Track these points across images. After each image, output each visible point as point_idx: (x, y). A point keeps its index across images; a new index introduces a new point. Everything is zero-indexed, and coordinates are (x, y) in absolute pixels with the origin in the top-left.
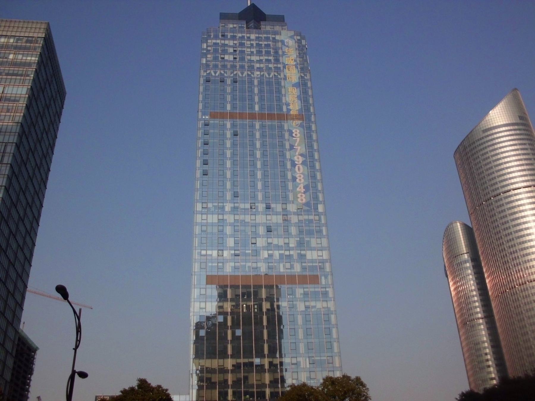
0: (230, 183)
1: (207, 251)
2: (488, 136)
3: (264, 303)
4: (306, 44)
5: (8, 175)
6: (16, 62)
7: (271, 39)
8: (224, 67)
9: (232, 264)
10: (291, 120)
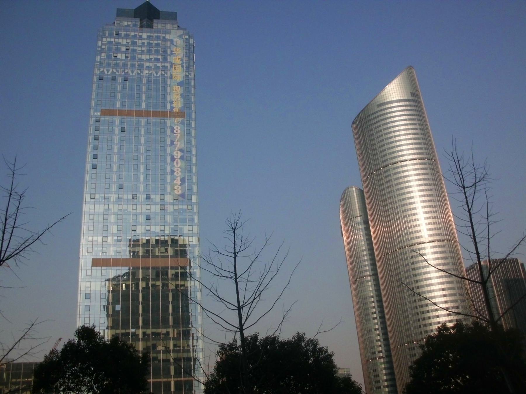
0: (116, 176)
2: (381, 110)
3: (140, 282)
9: (115, 249)
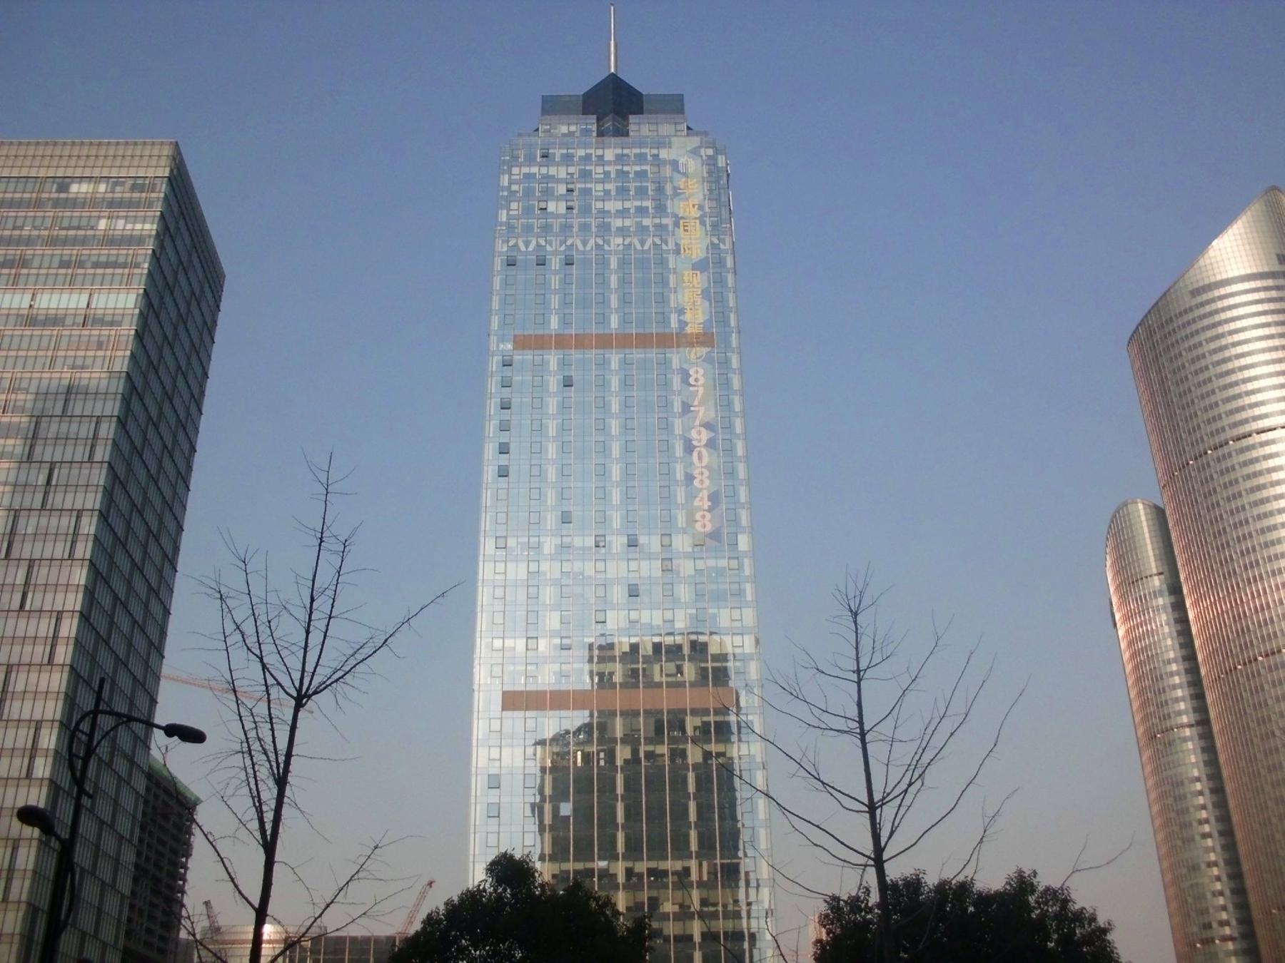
1: (506, 641)
2: (1202, 305)
4: (727, 164)
5: (105, 487)
6: (113, 235)
7: (649, 158)
8: (546, 229)
9: (556, 667)
10: (686, 347)
